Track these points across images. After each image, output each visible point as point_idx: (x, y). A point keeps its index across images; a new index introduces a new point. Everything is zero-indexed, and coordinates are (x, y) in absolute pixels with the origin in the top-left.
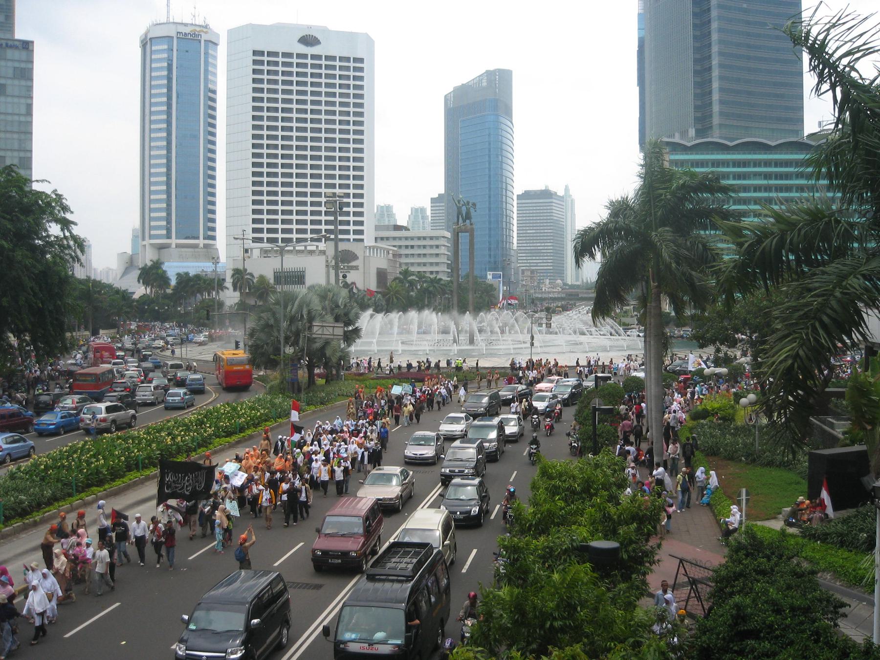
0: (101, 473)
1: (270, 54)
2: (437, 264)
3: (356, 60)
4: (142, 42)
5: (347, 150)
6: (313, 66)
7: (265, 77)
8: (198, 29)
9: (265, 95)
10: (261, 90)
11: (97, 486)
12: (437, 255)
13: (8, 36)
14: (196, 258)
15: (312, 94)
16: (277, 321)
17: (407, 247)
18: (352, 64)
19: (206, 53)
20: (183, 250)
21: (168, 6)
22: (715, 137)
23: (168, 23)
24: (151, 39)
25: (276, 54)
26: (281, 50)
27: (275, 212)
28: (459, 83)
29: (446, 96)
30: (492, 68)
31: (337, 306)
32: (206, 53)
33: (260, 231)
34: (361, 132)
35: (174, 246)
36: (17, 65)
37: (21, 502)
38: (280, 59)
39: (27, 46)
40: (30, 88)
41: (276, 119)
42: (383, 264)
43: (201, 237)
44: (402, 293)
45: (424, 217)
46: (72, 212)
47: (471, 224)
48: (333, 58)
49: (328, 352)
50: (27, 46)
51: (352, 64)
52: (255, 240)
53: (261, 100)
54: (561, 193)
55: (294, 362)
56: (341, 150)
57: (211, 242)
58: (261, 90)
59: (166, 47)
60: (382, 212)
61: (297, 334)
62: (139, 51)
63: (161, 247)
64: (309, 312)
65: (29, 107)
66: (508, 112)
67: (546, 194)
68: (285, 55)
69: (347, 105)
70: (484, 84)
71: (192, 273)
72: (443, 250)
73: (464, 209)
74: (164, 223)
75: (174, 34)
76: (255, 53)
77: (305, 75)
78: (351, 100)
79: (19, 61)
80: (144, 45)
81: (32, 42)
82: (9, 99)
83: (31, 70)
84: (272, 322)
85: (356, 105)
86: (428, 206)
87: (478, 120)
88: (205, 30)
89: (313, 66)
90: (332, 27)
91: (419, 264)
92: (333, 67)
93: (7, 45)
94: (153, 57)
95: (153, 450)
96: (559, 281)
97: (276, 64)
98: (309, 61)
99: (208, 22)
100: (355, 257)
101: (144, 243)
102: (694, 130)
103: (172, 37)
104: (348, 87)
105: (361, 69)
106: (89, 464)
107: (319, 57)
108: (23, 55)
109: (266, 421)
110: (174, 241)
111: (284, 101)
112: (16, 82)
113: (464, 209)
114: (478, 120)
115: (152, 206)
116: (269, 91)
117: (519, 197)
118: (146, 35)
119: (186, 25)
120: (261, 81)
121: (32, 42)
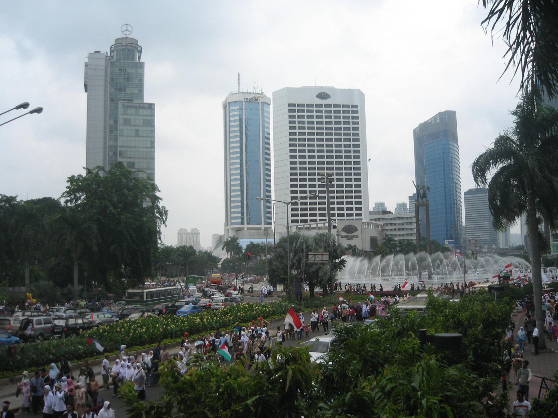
0: (144, 337)
1: (299, 105)
3: (353, 106)
4: (224, 105)
5: (350, 163)
6: (326, 111)
7: (297, 120)
8: (257, 96)
9: (297, 131)
10: (295, 128)
11: (139, 345)
13: (140, 102)
14: (259, 236)
15: (328, 129)
16: (286, 253)
17: (391, 224)
18: (350, 109)
19: (263, 110)
20: (252, 231)
21: (239, 83)
23: (239, 93)
25: (303, 105)
26: (306, 103)
28: (422, 122)
29: (414, 130)
30: (443, 111)
31: (329, 246)
32: (263, 110)
33: (297, 215)
34: (358, 151)
35: (246, 229)
36: (145, 118)
37: (79, 350)
38: (306, 108)
39: (151, 107)
40: (153, 132)
41: (304, 145)
42: (375, 234)
43: (263, 223)
44: (383, 247)
45: (405, 209)
46: (159, 191)
47: (427, 201)
48: (339, 106)
49: (321, 274)
50: (151, 107)
51: (350, 109)
52: (293, 221)
53: (295, 134)
55: (299, 281)
56: (346, 163)
58: (295, 128)
59: (238, 107)
60: (379, 207)
61: (299, 261)
62: (222, 111)
63: (238, 230)
64: (307, 247)
65: (153, 143)
66: (455, 137)
68: (308, 105)
69: (348, 134)
70: (438, 121)
71: (255, 243)
74: (240, 215)
75: (243, 99)
76: (290, 105)
77: (321, 117)
78: (351, 132)
79: (146, 116)
80: (225, 107)
81: (154, 104)
82: (141, 139)
83: (153, 120)
84: (283, 254)
85: (354, 134)
86: (407, 201)
89: (326, 111)
90: (337, 87)
91: (400, 235)
92: (339, 112)
93: (139, 106)
94: (231, 114)
95: (184, 326)
96: (494, 246)
97: (303, 111)
98: (324, 109)
99: (263, 91)
100: (356, 229)
101: (228, 228)
104: (349, 123)
105: (357, 112)
106: (135, 330)
107: (330, 106)
108: (149, 112)
109: (273, 315)
110: (246, 226)
111: (309, 134)
112: (145, 128)
115: (232, 205)
116: (300, 128)
117: (466, 193)
118: (226, 101)
119: (250, 93)
120: (294, 122)
121: (154, 104)
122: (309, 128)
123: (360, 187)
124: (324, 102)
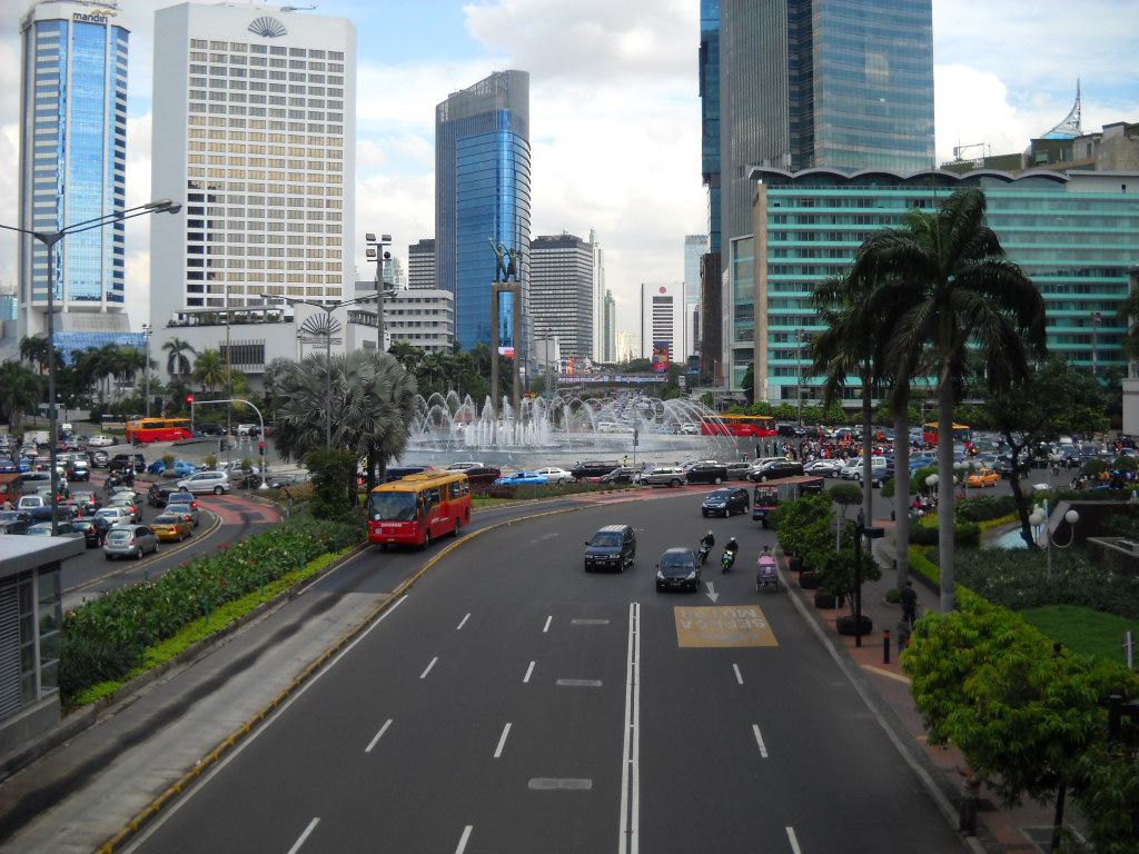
2: (435, 336)
4: (23, 25)
8: (103, 10)
12: (435, 324)
22: (823, 164)
24: (36, 22)
27: (299, 253)
54: (586, 240)
57: (118, 304)
67: (568, 241)
72: (441, 318)
73: (506, 262)
87: (479, 138)
88: (112, 11)
98: (268, 56)
101: (23, 306)
102: (790, 155)
103: (67, 21)
107: (281, 50)
113: (506, 262)
114: (479, 138)
122: (320, 116)
123: (190, 195)
124: (268, 42)
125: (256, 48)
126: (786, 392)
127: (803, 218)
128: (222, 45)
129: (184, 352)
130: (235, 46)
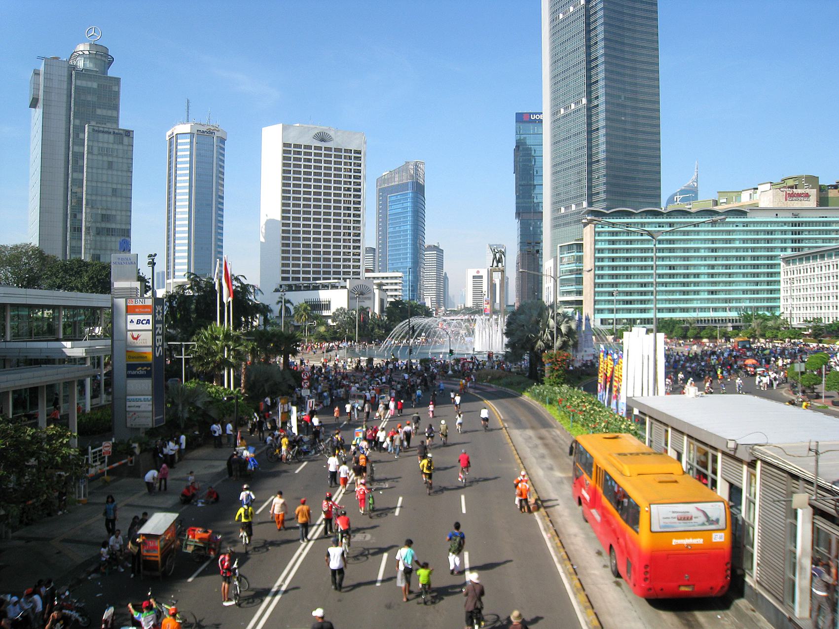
73: (498, 256)
98: (323, 152)
107: (329, 149)
113: (498, 256)
125: (316, 148)
126: (603, 321)
127: (794, 233)
128: (300, 146)
129: (288, 305)
130: (306, 147)
